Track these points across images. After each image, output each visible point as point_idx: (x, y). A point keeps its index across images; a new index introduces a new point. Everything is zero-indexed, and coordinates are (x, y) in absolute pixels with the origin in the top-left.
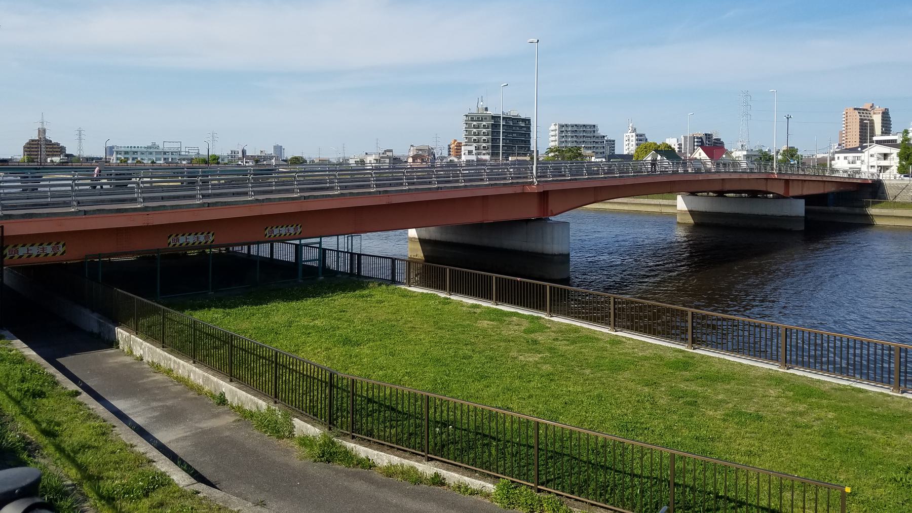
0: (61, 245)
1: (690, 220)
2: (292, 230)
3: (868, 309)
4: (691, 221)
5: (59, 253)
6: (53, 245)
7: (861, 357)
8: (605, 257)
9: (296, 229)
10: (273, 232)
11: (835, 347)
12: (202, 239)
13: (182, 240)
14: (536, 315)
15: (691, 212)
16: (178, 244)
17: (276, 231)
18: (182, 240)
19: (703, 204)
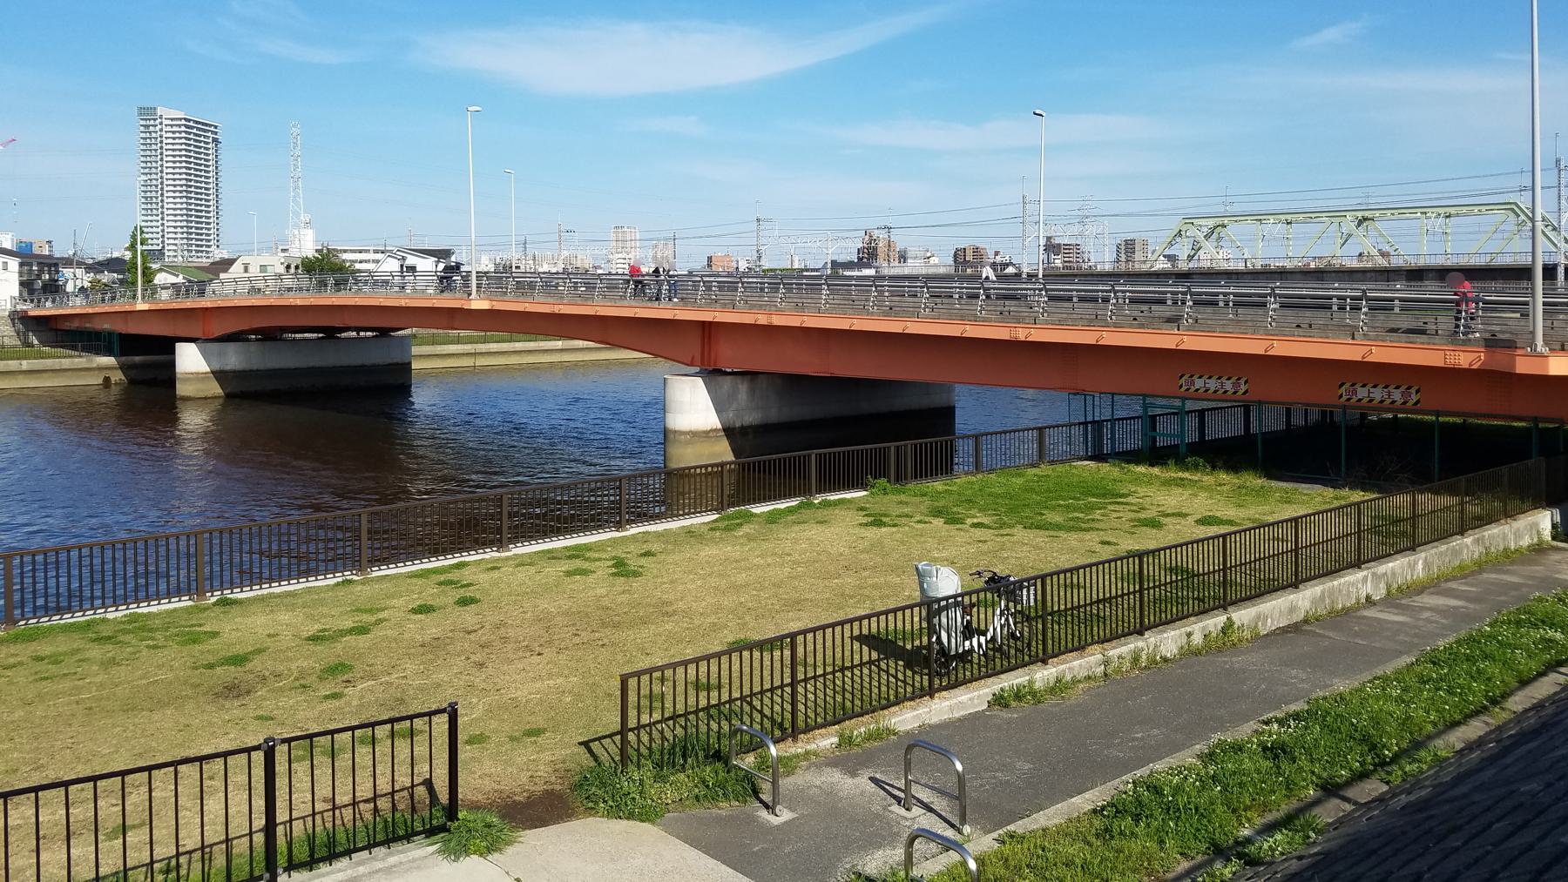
0: (1413, 391)
1: (215, 389)
2: (1228, 386)
3: (906, 510)
4: (219, 391)
5: (1411, 403)
6: (1403, 389)
7: (22, 589)
8: (94, 443)
9: (1405, 394)
10: (1193, 383)
11: (147, 572)
12: (1397, 396)
13: (1362, 393)
14: (782, 506)
15: (219, 375)
16: (1355, 399)
17: (1199, 383)
18: (1362, 393)
19: (234, 357)
